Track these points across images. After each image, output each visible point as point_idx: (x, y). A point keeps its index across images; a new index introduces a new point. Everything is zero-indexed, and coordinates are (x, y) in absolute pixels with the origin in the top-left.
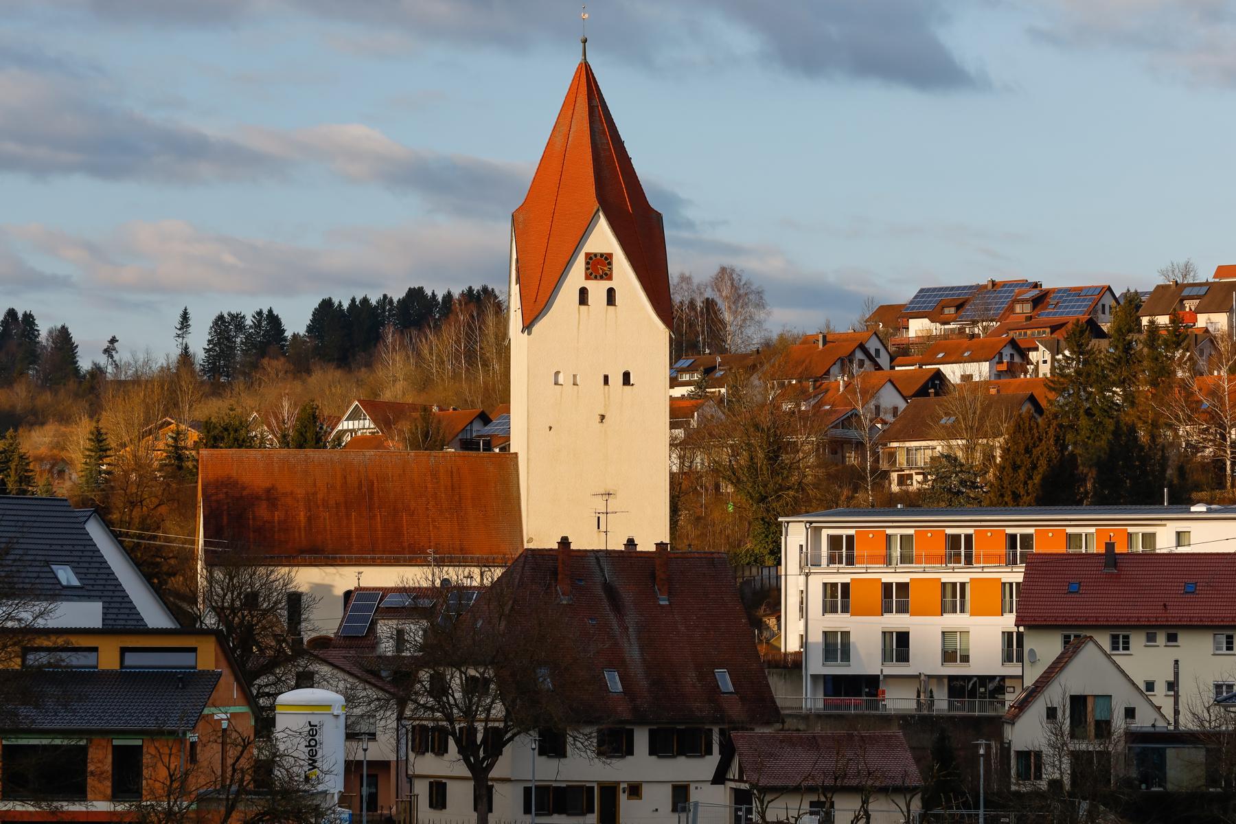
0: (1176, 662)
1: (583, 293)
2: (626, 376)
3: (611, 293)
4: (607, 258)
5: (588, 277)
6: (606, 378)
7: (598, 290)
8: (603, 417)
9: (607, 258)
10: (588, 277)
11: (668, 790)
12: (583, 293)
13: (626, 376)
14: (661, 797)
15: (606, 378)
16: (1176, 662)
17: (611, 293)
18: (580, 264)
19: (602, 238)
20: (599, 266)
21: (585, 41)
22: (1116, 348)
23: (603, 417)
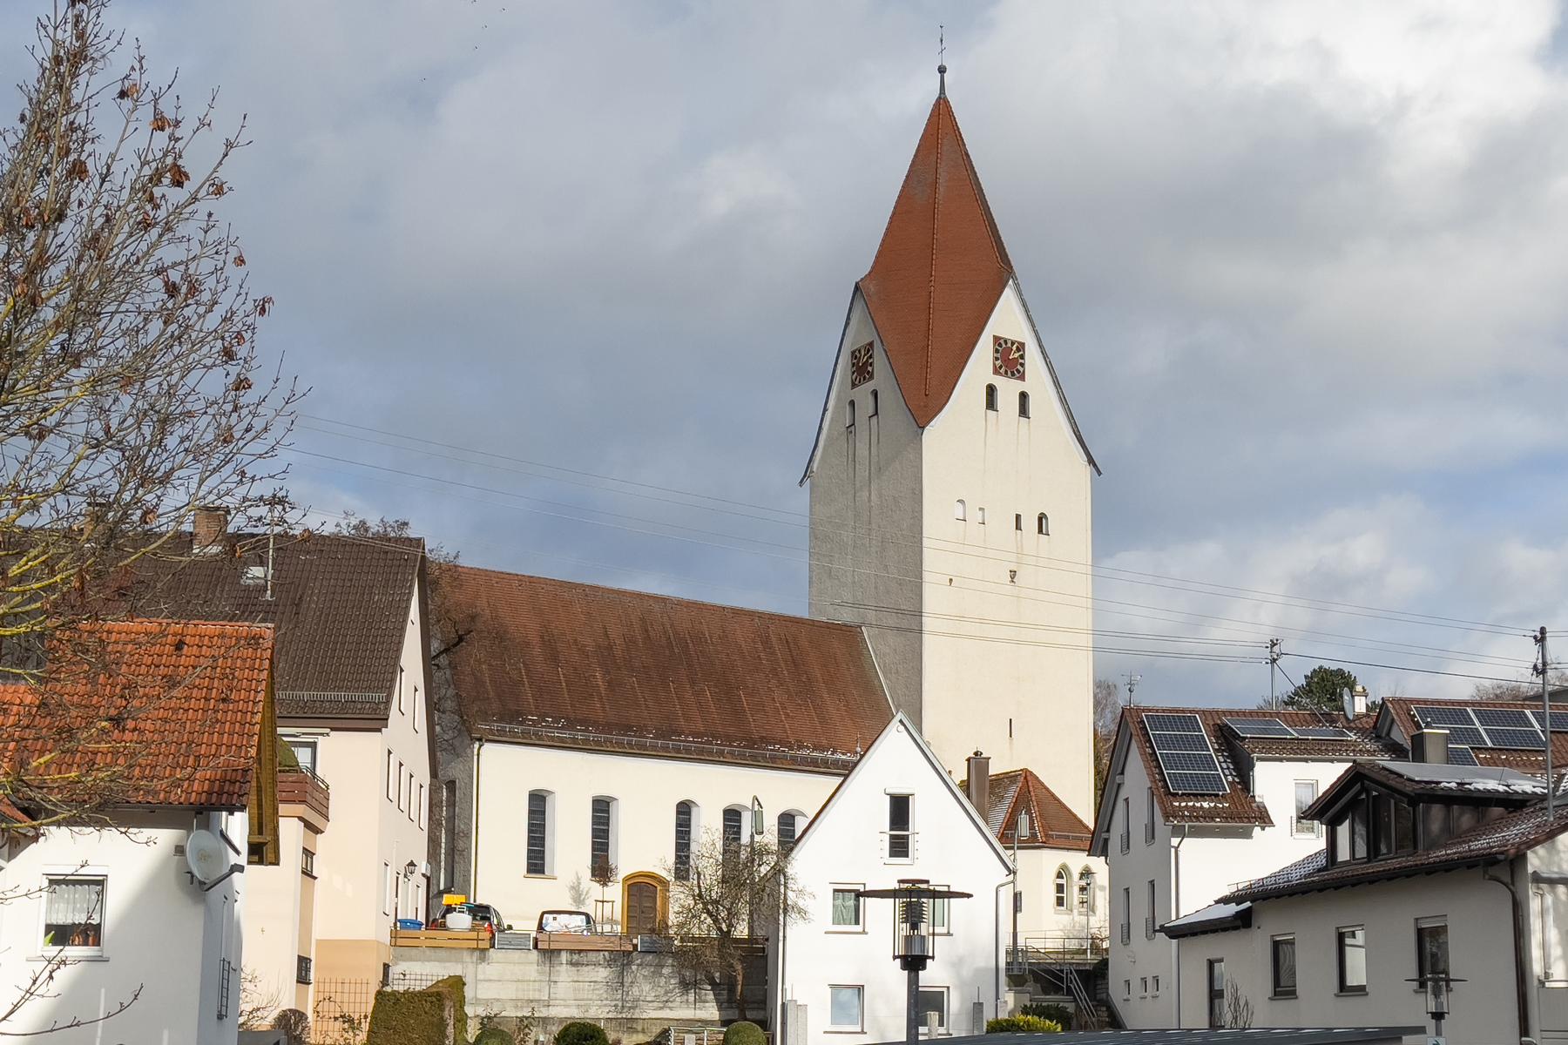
0: (899, 847)
1: (991, 390)
2: (1042, 518)
3: (1023, 396)
7: (1008, 390)
8: (1013, 574)
10: (996, 371)
12: (991, 390)
16: (899, 847)
17: (1023, 396)
18: (983, 354)
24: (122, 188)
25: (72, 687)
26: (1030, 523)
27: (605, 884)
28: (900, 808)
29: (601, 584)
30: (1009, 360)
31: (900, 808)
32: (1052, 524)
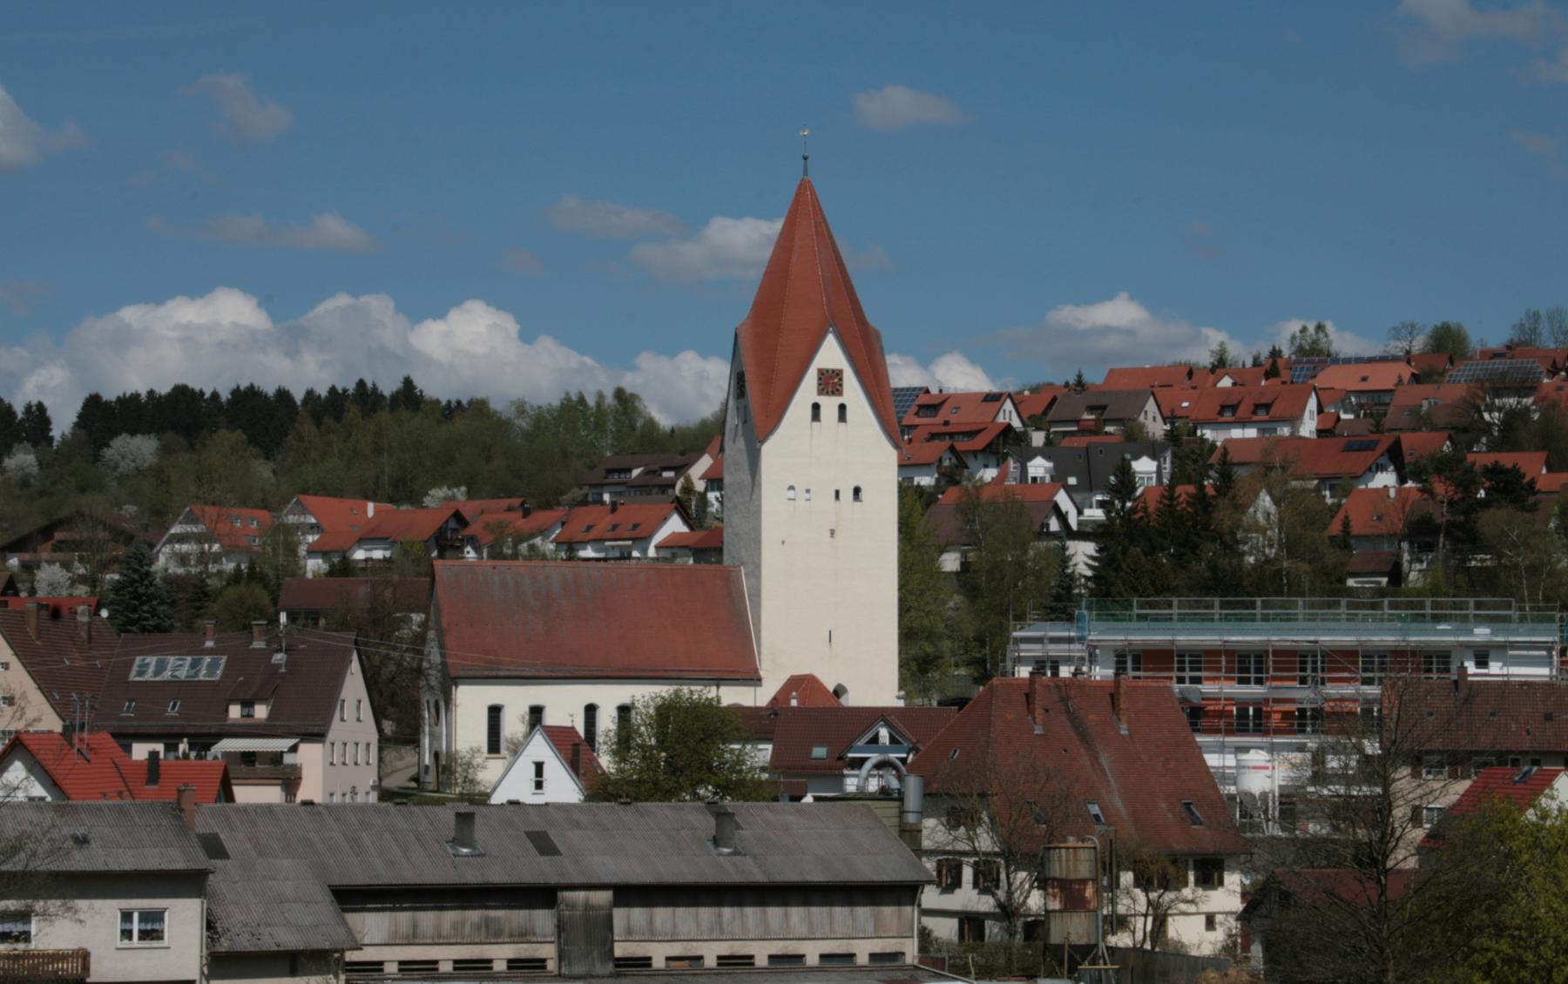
0: (539, 785)
1: (816, 407)
2: (857, 491)
3: (842, 408)
4: (838, 374)
5: (820, 392)
6: (837, 493)
7: (829, 405)
8: (832, 532)
9: (838, 374)
10: (820, 392)
11: (1203, 919)
12: (816, 407)
13: (857, 491)
14: (361, 791)
15: (837, 493)
16: (539, 785)
17: (842, 408)
18: (810, 380)
19: (831, 354)
20: (830, 382)
21: (805, 158)
22: (1034, 560)
23: (832, 532)
24: (1301, 748)
25: (193, 755)
26: (847, 495)
27: (41, 407)
28: (539, 767)
29: (526, 946)
30: (830, 382)
31: (539, 767)
32: (863, 495)
